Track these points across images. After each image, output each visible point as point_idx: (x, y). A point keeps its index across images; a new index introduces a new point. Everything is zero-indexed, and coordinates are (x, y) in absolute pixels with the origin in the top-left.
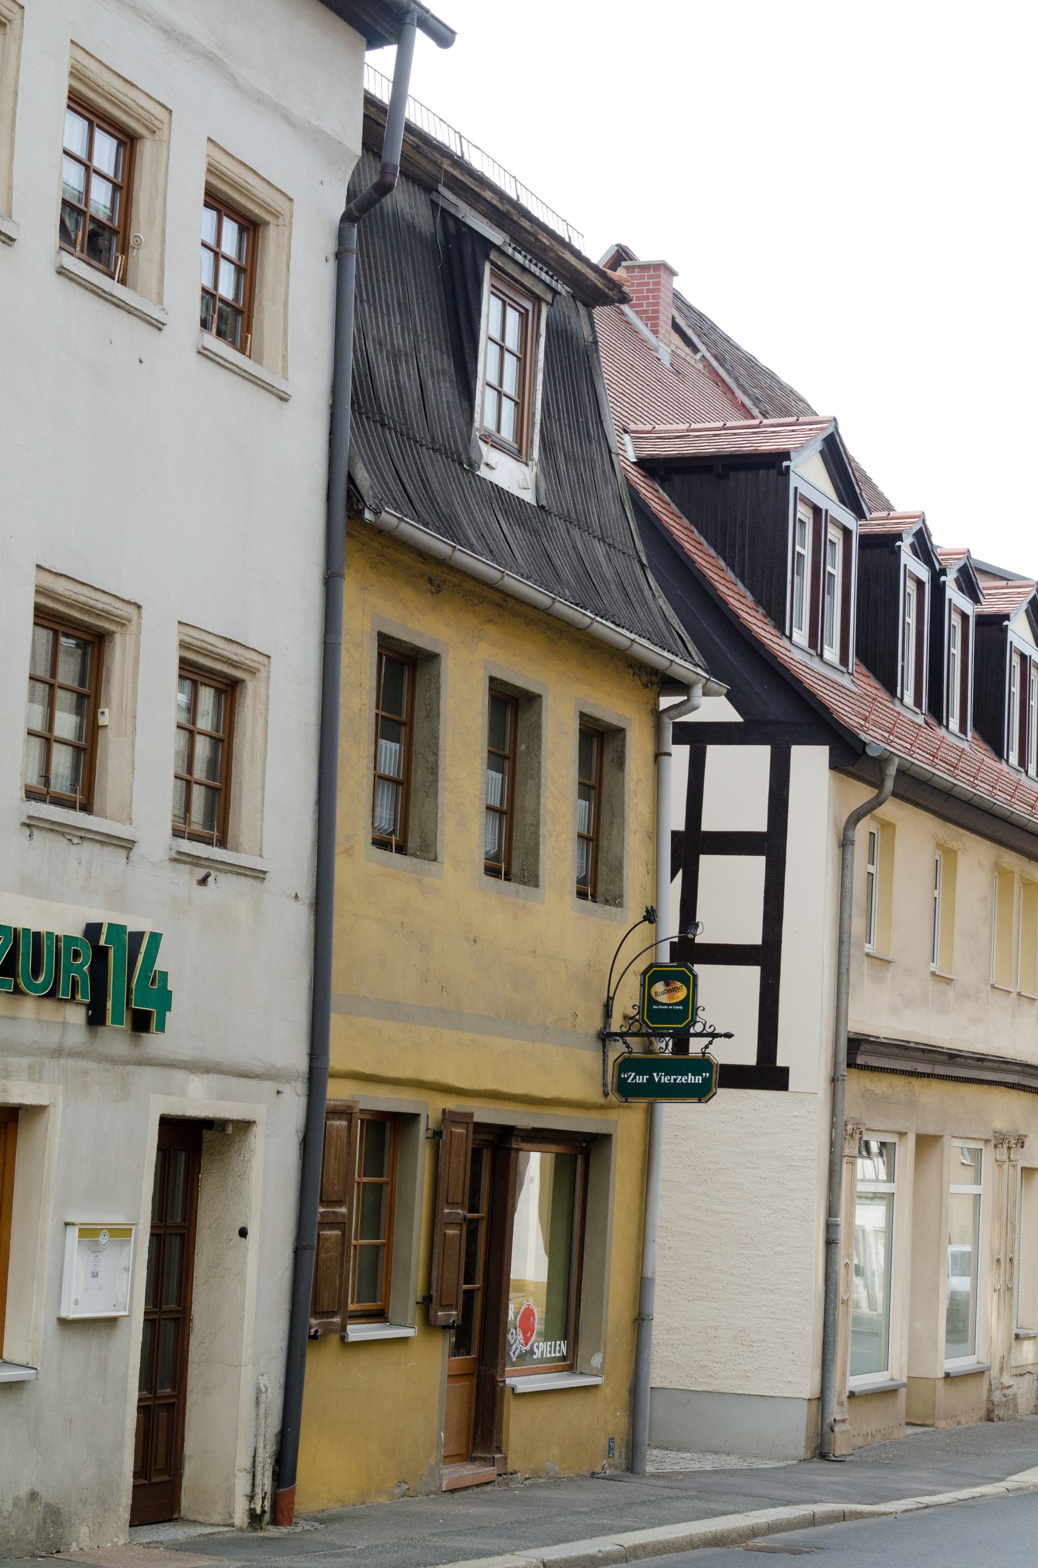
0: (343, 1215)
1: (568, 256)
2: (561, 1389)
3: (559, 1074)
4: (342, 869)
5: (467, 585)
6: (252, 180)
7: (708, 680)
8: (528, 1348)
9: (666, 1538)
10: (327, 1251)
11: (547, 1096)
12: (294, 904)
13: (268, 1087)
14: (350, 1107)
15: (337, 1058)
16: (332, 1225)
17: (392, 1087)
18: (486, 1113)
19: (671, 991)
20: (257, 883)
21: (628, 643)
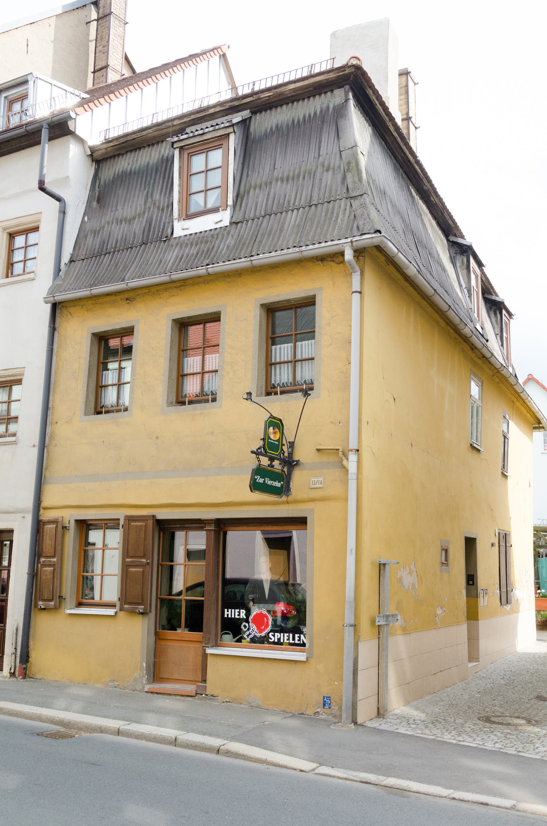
0: (54, 562)
1: (292, 86)
2: (263, 658)
3: (230, 491)
4: (61, 430)
5: (153, 289)
6: (18, 220)
7: (352, 242)
8: (263, 634)
9: (20, 709)
10: (46, 576)
11: (218, 502)
12: (33, 449)
13: (19, 516)
14: (56, 519)
15: (45, 503)
16: (50, 566)
17: (99, 509)
18: (163, 514)
19: (275, 433)
20: (14, 446)
21: (249, 263)
